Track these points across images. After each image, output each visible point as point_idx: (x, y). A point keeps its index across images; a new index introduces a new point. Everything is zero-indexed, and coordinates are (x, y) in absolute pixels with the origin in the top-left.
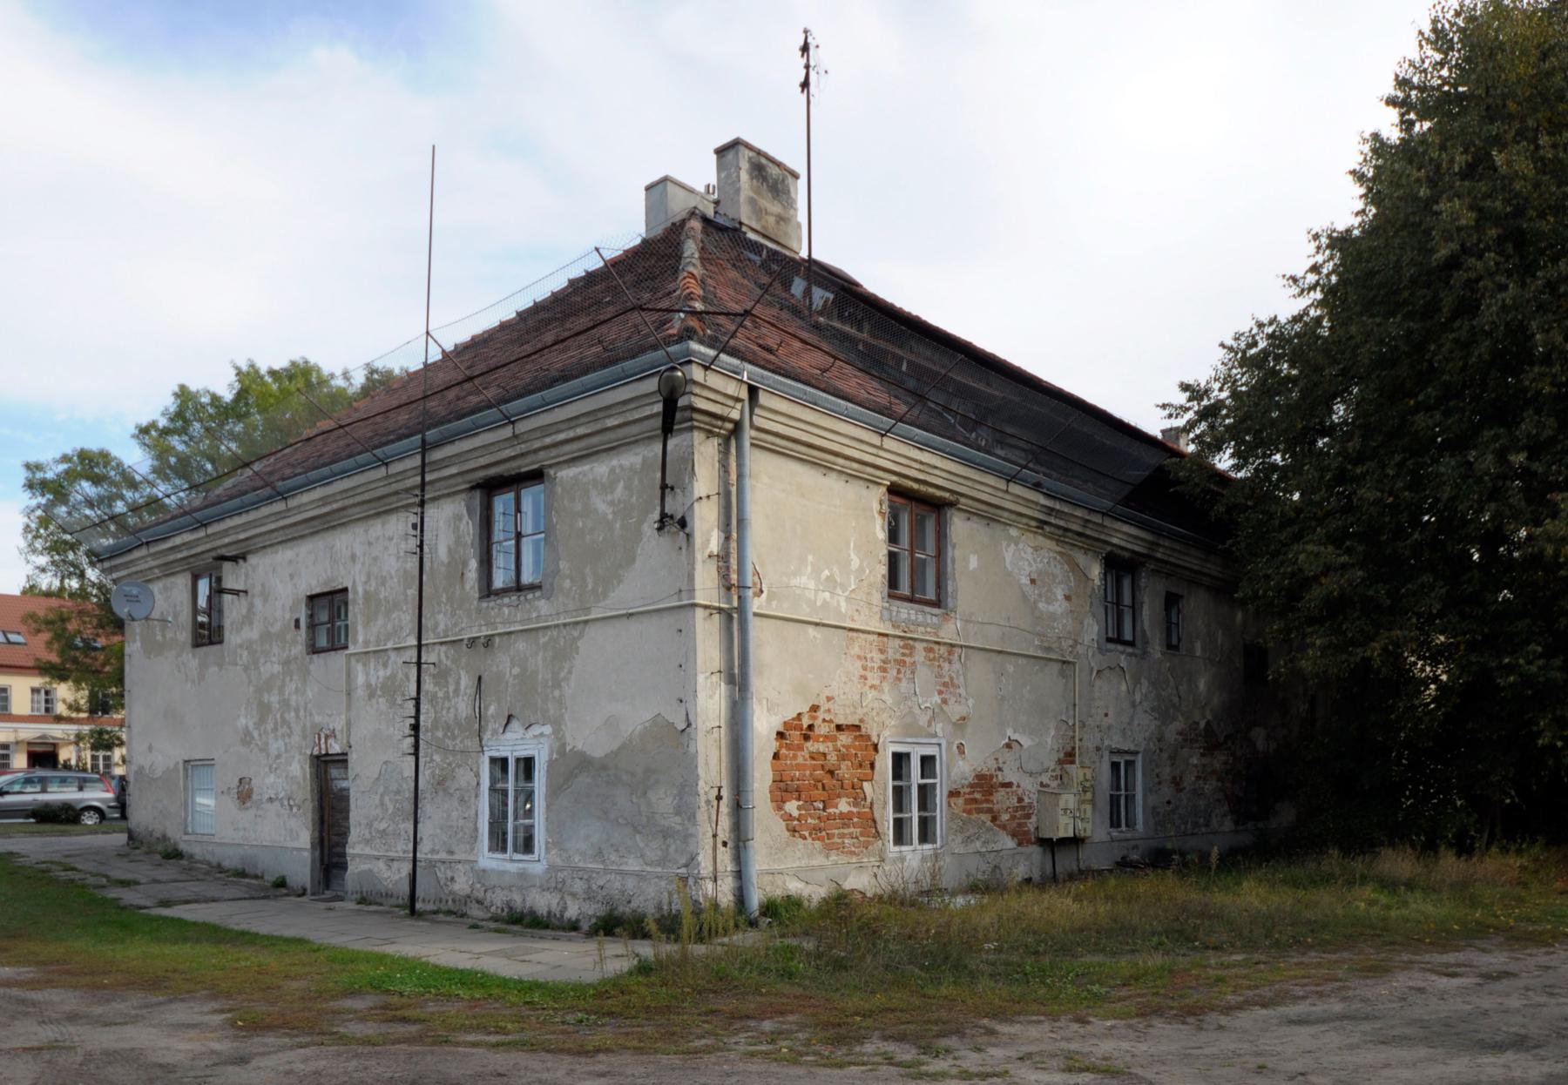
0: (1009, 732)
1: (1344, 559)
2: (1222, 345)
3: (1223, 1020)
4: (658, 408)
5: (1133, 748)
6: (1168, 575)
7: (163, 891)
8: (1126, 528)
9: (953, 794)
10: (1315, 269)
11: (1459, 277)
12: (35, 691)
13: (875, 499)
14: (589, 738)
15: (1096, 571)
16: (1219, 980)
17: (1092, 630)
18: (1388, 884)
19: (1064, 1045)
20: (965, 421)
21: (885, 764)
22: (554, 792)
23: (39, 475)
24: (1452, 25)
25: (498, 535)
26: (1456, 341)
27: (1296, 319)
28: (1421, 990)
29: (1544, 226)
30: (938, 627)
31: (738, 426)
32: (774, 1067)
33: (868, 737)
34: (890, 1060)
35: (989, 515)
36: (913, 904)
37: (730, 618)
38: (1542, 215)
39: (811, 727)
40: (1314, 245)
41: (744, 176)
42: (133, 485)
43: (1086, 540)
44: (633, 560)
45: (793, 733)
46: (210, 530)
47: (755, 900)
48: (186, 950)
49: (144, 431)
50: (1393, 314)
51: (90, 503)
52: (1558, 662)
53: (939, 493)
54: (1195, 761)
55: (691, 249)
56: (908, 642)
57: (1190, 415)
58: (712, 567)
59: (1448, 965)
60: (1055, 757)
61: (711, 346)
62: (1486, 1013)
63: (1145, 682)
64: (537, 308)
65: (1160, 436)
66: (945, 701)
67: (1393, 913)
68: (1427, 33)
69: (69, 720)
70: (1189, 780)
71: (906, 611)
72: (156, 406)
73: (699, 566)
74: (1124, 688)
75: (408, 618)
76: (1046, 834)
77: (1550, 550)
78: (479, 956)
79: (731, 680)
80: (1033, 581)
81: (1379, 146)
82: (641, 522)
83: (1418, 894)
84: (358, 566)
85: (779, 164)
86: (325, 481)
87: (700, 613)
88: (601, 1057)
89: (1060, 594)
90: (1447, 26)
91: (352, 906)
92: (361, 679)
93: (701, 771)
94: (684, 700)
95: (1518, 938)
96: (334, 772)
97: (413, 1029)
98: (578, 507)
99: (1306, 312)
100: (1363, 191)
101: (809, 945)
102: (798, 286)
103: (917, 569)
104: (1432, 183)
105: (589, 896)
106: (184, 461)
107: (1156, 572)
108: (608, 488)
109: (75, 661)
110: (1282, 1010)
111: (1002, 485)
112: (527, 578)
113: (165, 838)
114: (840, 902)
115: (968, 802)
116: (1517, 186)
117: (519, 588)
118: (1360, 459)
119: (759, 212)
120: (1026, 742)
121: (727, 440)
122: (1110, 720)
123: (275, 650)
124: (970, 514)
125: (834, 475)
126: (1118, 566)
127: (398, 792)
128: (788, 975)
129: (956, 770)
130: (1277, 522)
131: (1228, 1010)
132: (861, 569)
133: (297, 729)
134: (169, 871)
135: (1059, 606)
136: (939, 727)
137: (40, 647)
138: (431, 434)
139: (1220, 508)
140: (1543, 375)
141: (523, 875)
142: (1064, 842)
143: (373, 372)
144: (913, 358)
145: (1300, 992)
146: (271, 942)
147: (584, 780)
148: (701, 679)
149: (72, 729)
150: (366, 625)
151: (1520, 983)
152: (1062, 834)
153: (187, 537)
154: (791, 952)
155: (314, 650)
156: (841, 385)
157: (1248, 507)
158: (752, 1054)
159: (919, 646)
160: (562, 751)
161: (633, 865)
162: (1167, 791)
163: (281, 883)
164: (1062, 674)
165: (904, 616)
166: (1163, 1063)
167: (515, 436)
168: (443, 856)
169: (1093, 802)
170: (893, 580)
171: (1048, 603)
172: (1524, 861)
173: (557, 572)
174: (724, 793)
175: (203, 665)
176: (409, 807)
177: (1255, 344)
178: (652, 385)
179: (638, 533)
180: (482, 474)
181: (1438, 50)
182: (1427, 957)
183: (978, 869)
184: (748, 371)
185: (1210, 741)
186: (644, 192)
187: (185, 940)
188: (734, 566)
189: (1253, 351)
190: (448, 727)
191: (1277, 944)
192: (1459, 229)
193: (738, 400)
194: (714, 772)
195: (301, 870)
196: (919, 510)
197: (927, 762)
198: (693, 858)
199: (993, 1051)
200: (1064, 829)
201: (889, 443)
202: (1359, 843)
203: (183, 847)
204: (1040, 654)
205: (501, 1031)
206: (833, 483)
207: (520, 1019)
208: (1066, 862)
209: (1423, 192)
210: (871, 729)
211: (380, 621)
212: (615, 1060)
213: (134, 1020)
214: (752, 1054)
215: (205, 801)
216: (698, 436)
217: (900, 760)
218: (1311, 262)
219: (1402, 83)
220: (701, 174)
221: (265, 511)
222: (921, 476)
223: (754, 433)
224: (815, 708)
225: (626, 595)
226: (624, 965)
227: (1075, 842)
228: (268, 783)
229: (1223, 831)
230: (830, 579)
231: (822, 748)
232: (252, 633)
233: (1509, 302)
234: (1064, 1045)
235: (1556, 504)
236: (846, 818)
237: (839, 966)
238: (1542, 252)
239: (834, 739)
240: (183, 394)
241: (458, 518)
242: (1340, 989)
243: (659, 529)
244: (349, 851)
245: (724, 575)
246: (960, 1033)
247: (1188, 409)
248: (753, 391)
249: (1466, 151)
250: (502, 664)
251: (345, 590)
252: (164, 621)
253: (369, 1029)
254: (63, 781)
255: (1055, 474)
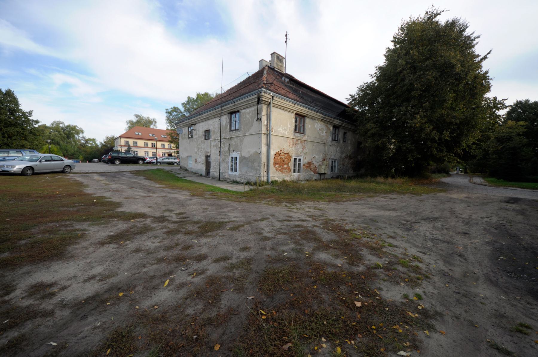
0: (314, 155)
1: (375, 126)
2: (357, 87)
3: (342, 203)
4: (257, 100)
5: (336, 158)
6: (345, 129)
7: (184, 175)
8: (337, 121)
9: (304, 165)
10: (376, 73)
11: (402, 74)
12: (168, 145)
13: (293, 115)
14: (245, 154)
15: (331, 128)
16: (343, 197)
17: (330, 138)
18: (378, 183)
19: (315, 205)
20: (310, 102)
21: (292, 160)
22: (240, 162)
23: (168, 111)
24: (405, 26)
25: (232, 121)
26: (400, 86)
27: (371, 83)
28: (378, 200)
29: (419, 65)
30: (303, 137)
31: (270, 103)
32: (267, 206)
33: (290, 155)
34: (286, 206)
35: (313, 118)
36: (295, 182)
37: (268, 135)
38: (419, 63)
39: (280, 153)
40: (376, 69)
41: (275, 59)
42: (181, 113)
43: (330, 123)
44: (253, 125)
45: (277, 154)
46: (191, 120)
47: (270, 180)
48: (186, 184)
49: (183, 104)
50: (389, 81)
51: (175, 115)
52: (413, 145)
53: (304, 114)
54: (347, 161)
55: (265, 72)
56: (297, 140)
57: (351, 100)
58: (265, 127)
59: (385, 197)
60: (322, 159)
61: (266, 89)
62: (389, 205)
63: (339, 147)
64: (241, 83)
65: (347, 104)
66: (303, 150)
67: (377, 188)
68: (400, 28)
69: (173, 149)
70: (345, 164)
71: (297, 135)
72: (185, 100)
73: (263, 127)
74: (335, 148)
75: (219, 134)
76: (319, 172)
77: (413, 125)
78: (228, 187)
79: (267, 145)
80: (320, 130)
81: (389, 50)
82: (254, 119)
83: (383, 185)
84: (212, 126)
85: (281, 56)
86: (207, 112)
87: (263, 134)
88: (242, 203)
89: (325, 132)
90: (404, 26)
91: (211, 179)
92: (212, 144)
93: (262, 160)
94: (260, 148)
95: (399, 193)
96: (209, 158)
97: (216, 197)
98: (244, 116)
99: (373, 81)
100: (386, 58)
101: (277, 188)
102: (283, 78)
103: (300, 127)
104: (398, 56)
105: (245, 179)
106: (189, 109)
107: (342, 128)
108: (249, 113)
109: (174, 140)
110: (353, 202)
111: (315, 113)
112: (237, 128)
113: (185, 167)
114: (284, 181)
115: (306, 166)
116: (414, 57)
117: (235, 130)
118: (381, 108)
119: (278, 65)
120: (317, 157)
121: (268, 105)
122: (332, 154)
123: (200, 139)
124: (309, 118)
125: (286, 111)
126: (335, 127)
127: (218, 162)
128: (273, 192)
129: (304, 161)
130: (364, 119)
131: (344, 202)
132: (290, 127)
133: (203, 152)
134: (186, 172)
135: (324, 134)
136: (302, 154)
137: (169, 138)
138: (222, 105)
139: (355, 117)
140: (416, 93)
141: (235, 175)
142: (322, 174)
143: (217, 94)
144: (302, 90)
145: (357, 199)
146: (198, 183)
147: (244, 161)
148: (262, 145)
149: (174, 151)
150: (213, 135)
151: (397, 200)
152: (322, 172)
153: (187, 121)
154: (274, 189)
155: (206, 139)
156: (288, 96)
157: (360, 117)
158: (265, 204)
159: (299, 141)
160: (241, 156)
161: (251, 174)
162: (341, 166)
163: (201, 175)
164: (324, 146)
165: (297, 135)
166: (330, 209)
167: (235, 105)
168: (224, 172)
169: (328, 167)
170: (295, 129)
171: (322, 133)
172: (404, 180)
173: (241, 127)
174: (266, 164)
175: (190, 141)
176: (219, 164)
177: (363, 87)
178: (256, 96)
179: (254, 121)
180: (230, 111)
181: (402, 31)
182: (382, 195)
183: (307, 177)
184: (272, 93)
185: (350, 158)
186: (259, 62)
187: (186, 182)
188: (269, 127)
189: (363, 88)
190: (225, 152)
191: (355, 192)
192: (402, 65)
193: (270, 98)
194: (264, 160)
195: (204, 173)
196: (301, 117)
197: (300, 160)
198: (260, 174)
199: (303, 205)
200: (322, 171)
201: (296, 106)
202: (374, 176)
203: (187, 169)
204: (320, 142)
205: (229, 198)
206: (286, 113)
207: (232, 196)
208: (322, 177)
209: (396, 58)
210: (290, 154)
211: (215, 135)
212: (244, 203)
213: (177, 193)
214: (265, 204)
215: (191, 162)
216: (263, 105)
217: (295, 159)
218: (375, 72)
219: (395, 38)
220: (268, 59)
221: (198, 117)
222: (301, 112)
223: (273, 104)
224: (281, 150)
225: (252, 131)
226: (248, 189)
227: (324, 174)
228: (199, 160)
229: (351, 173)
230: (285, 129)
231: (282, 157)
232: (197, 136)
233: (411, 79)
234: (315, 205)
235: (416, 117)
236: (285, 168)
237: (281, 191)
238: (418, 69)
239: (284, 155)
240: (189, 98)
241: (226, 118)
242: (364, 199)
243: (257, 120)
244: (211, 170)
245: (267, 128)
246: (298, 202)
247: (350, 99)
248: (273, 97)
249: (405, 50)
250: (233, 142)
251: (210, 130)
252: (184, 134)
253: (210, 197)
254: (172, 158)
255: (325, 111)
